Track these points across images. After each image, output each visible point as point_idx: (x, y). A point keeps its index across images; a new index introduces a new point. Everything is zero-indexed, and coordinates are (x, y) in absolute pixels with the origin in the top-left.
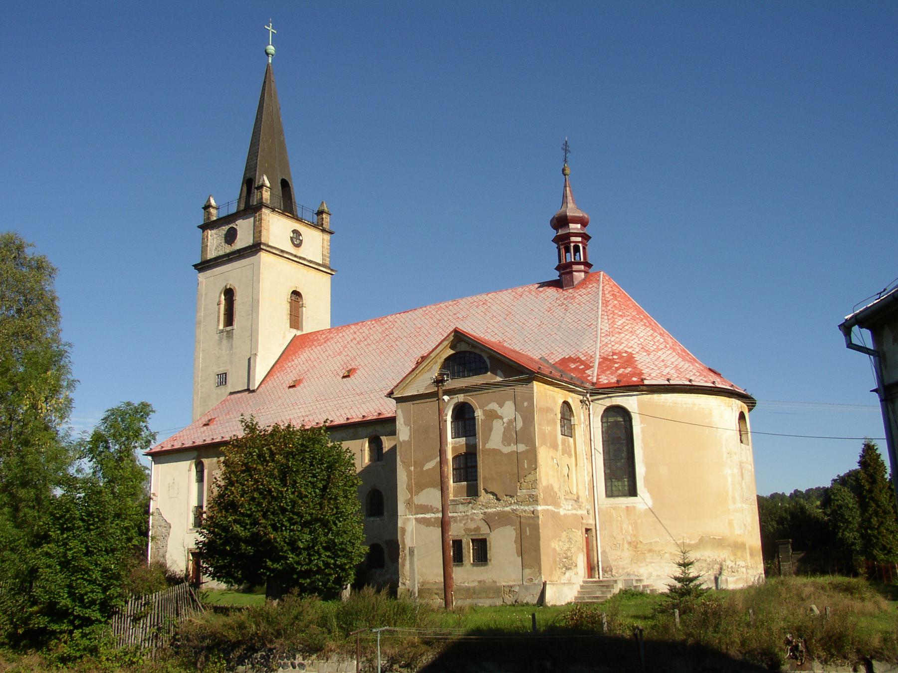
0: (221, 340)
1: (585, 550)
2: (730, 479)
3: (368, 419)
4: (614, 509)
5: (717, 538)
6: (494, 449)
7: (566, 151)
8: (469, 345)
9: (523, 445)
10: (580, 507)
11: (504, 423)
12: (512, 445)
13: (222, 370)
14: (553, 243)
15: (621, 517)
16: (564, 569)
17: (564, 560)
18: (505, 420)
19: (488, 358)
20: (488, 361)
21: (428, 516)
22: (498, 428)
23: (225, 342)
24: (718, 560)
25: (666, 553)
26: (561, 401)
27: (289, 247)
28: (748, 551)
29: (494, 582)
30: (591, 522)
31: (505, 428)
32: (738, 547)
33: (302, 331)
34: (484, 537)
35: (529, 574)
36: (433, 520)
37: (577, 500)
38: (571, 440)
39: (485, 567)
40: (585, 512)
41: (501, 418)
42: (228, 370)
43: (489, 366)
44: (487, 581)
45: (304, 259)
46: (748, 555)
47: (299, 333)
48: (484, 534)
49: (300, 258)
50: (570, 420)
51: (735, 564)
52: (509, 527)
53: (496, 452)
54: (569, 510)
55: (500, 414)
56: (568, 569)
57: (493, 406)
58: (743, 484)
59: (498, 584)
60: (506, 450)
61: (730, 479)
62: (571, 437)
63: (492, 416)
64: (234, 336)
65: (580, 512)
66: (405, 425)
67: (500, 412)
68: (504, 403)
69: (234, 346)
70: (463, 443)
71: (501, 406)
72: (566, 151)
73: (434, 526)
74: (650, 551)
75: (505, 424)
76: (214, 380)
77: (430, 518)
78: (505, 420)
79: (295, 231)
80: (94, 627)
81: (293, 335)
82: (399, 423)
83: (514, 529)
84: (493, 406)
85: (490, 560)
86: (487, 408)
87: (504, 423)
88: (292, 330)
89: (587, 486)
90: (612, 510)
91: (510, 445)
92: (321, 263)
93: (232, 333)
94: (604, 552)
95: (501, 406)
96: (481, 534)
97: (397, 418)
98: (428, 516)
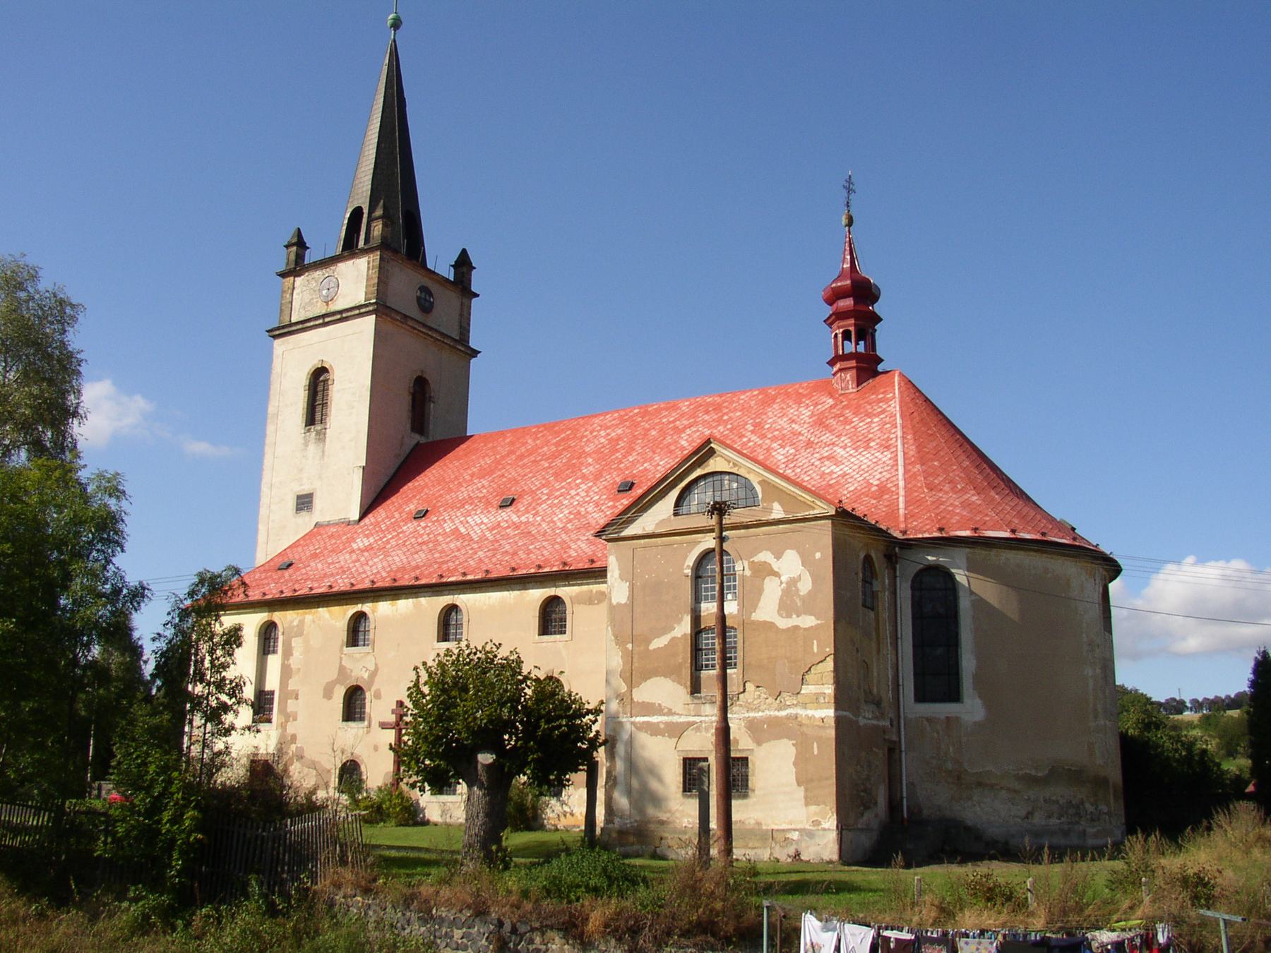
0: (306, 444)
1: (887, 781)
2: (1091, 683)
3: (545, 570)
4: (928, 720)
5: (1073, 769)
6: (765, 622)
7: (850, 190)
8: (729, 462)
9: (813, 618)
10: (882, 716)
11: (781, 583)
12: (794, 616)
13: (305, 490)
14: (882, 317)
15: (938, 733)
16: (862, 808)
17: (862, 794)
18: (784, 578)
19: (759, 483)
20: (758, 489)
21: (655, 719)
22: (772, 591)
23: (312, 447)
24: (1074, 803)
25: (1002, 788)
26: (862, 555)
27: (414, 312)
28: (1111, 791)
29: (759, 824)
30: (894, 738)
31: (782, 590)
32: (1100, 783)
33: (428, 437)
34: (744, 755)
35: (815, 814)
36: (662, 726)
37: (878, 703)
38: (872, 614)
39: (745, 801)
40: (887, 724)
41: (777, 575)
42: (315, 489)
43: (760, 496)
44: (747, 822)
45: (436, 331)
46: (1112, 796)
47: (423, 440)
48: (743, 750)
49: (431, 329)
50: (871, 584)
51: (1096, 809)
52: (785, 741)
53: (770, 626)
54: (869, 719)
55: (776, 569)
56: (867, 808)
57: (765, 556)
58: (1107, 691)
59: (764, 827)
60: (783, 623)
61: (1091, 683)
62: (873, 609)
63: (764, 571)
64: (327, 440)
65: (882, 723)
66: (622, 580)
67: (776, 565)
68: (783, 553)
69: (326, 454)
70: (712, 611)
71: (778, 556)
72: (850, 190)
73: (663, 736)
74: (979, 784)
75: (784, 585)
76: (291, 503)
77: (658, 723)
78: (784, 578)
79: (423, 289)
80: (1142, 842)
81: (416, 441)
82: (612, 576)
83: (793, 744)
84: (765, 556)
85: (753, 791)
86: (756, 559)
87: (781, 583)
88: (413, 435)
89: (890, 683)
90: (925, 722)
91: (791, 617)
92: (458, 338)
93: (325, 434)
94: (911, 785)
95: (778, 556)
96: (740, 750)
97: (609, 569)
98: (655, 719)
